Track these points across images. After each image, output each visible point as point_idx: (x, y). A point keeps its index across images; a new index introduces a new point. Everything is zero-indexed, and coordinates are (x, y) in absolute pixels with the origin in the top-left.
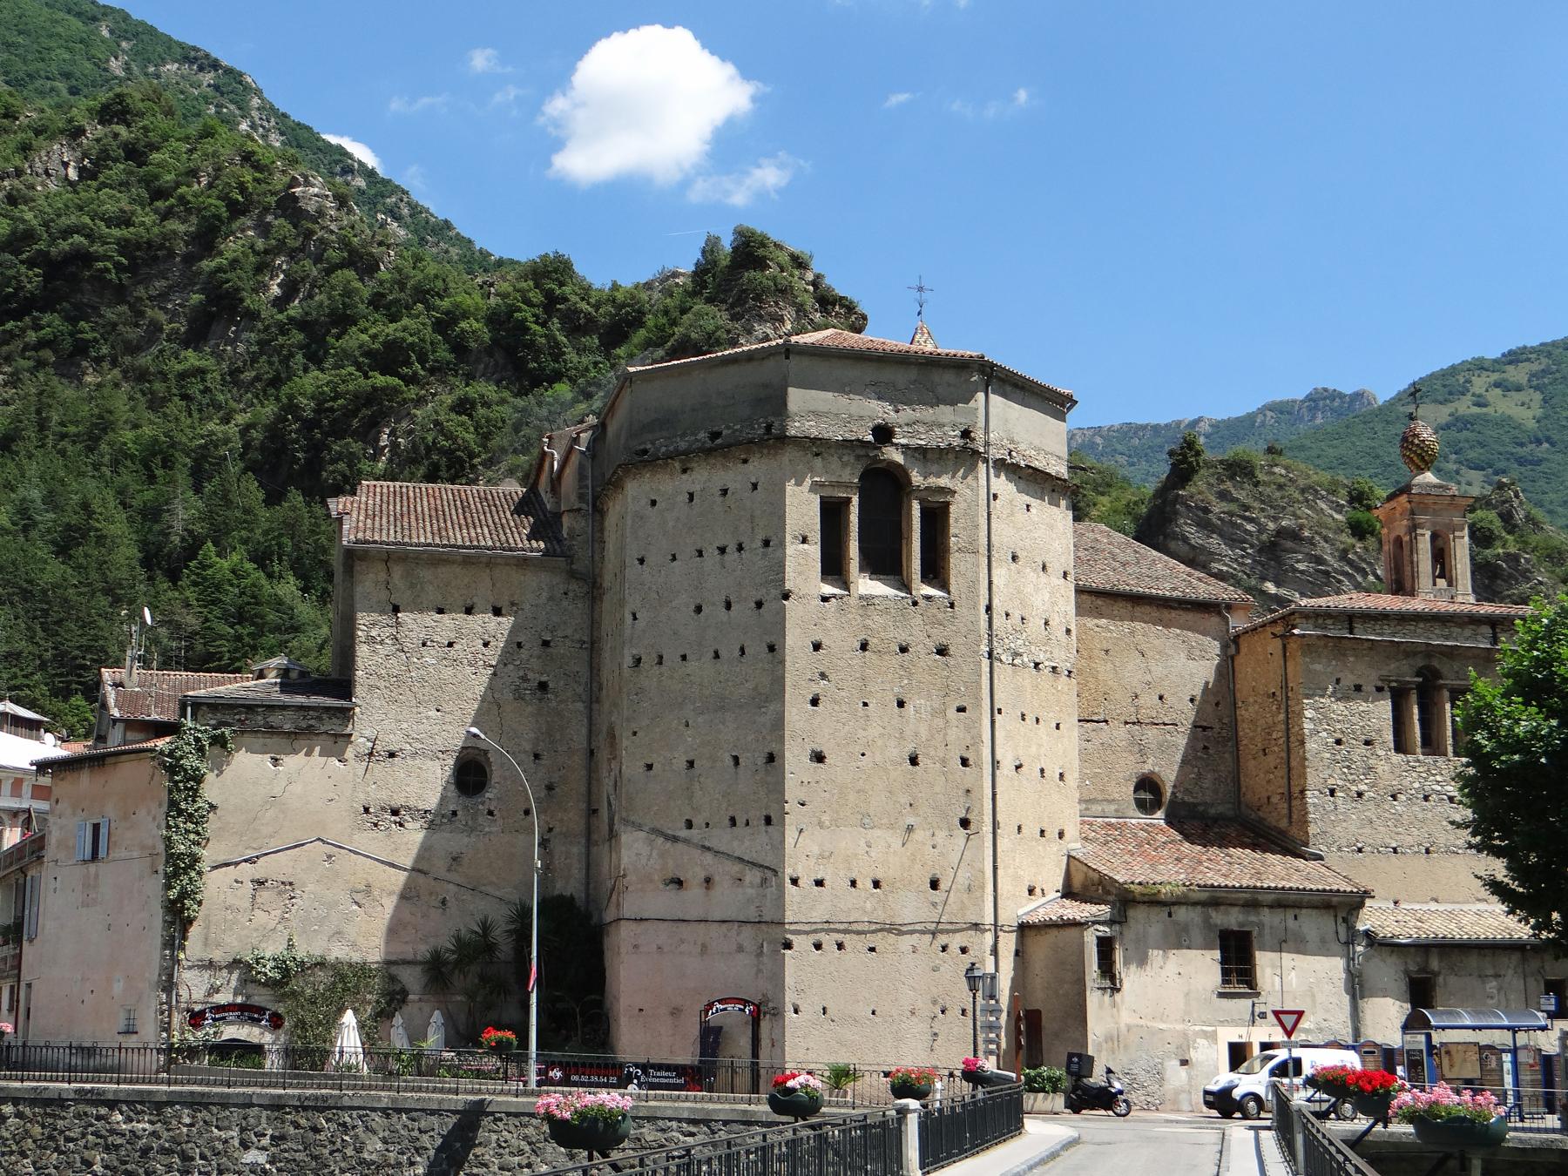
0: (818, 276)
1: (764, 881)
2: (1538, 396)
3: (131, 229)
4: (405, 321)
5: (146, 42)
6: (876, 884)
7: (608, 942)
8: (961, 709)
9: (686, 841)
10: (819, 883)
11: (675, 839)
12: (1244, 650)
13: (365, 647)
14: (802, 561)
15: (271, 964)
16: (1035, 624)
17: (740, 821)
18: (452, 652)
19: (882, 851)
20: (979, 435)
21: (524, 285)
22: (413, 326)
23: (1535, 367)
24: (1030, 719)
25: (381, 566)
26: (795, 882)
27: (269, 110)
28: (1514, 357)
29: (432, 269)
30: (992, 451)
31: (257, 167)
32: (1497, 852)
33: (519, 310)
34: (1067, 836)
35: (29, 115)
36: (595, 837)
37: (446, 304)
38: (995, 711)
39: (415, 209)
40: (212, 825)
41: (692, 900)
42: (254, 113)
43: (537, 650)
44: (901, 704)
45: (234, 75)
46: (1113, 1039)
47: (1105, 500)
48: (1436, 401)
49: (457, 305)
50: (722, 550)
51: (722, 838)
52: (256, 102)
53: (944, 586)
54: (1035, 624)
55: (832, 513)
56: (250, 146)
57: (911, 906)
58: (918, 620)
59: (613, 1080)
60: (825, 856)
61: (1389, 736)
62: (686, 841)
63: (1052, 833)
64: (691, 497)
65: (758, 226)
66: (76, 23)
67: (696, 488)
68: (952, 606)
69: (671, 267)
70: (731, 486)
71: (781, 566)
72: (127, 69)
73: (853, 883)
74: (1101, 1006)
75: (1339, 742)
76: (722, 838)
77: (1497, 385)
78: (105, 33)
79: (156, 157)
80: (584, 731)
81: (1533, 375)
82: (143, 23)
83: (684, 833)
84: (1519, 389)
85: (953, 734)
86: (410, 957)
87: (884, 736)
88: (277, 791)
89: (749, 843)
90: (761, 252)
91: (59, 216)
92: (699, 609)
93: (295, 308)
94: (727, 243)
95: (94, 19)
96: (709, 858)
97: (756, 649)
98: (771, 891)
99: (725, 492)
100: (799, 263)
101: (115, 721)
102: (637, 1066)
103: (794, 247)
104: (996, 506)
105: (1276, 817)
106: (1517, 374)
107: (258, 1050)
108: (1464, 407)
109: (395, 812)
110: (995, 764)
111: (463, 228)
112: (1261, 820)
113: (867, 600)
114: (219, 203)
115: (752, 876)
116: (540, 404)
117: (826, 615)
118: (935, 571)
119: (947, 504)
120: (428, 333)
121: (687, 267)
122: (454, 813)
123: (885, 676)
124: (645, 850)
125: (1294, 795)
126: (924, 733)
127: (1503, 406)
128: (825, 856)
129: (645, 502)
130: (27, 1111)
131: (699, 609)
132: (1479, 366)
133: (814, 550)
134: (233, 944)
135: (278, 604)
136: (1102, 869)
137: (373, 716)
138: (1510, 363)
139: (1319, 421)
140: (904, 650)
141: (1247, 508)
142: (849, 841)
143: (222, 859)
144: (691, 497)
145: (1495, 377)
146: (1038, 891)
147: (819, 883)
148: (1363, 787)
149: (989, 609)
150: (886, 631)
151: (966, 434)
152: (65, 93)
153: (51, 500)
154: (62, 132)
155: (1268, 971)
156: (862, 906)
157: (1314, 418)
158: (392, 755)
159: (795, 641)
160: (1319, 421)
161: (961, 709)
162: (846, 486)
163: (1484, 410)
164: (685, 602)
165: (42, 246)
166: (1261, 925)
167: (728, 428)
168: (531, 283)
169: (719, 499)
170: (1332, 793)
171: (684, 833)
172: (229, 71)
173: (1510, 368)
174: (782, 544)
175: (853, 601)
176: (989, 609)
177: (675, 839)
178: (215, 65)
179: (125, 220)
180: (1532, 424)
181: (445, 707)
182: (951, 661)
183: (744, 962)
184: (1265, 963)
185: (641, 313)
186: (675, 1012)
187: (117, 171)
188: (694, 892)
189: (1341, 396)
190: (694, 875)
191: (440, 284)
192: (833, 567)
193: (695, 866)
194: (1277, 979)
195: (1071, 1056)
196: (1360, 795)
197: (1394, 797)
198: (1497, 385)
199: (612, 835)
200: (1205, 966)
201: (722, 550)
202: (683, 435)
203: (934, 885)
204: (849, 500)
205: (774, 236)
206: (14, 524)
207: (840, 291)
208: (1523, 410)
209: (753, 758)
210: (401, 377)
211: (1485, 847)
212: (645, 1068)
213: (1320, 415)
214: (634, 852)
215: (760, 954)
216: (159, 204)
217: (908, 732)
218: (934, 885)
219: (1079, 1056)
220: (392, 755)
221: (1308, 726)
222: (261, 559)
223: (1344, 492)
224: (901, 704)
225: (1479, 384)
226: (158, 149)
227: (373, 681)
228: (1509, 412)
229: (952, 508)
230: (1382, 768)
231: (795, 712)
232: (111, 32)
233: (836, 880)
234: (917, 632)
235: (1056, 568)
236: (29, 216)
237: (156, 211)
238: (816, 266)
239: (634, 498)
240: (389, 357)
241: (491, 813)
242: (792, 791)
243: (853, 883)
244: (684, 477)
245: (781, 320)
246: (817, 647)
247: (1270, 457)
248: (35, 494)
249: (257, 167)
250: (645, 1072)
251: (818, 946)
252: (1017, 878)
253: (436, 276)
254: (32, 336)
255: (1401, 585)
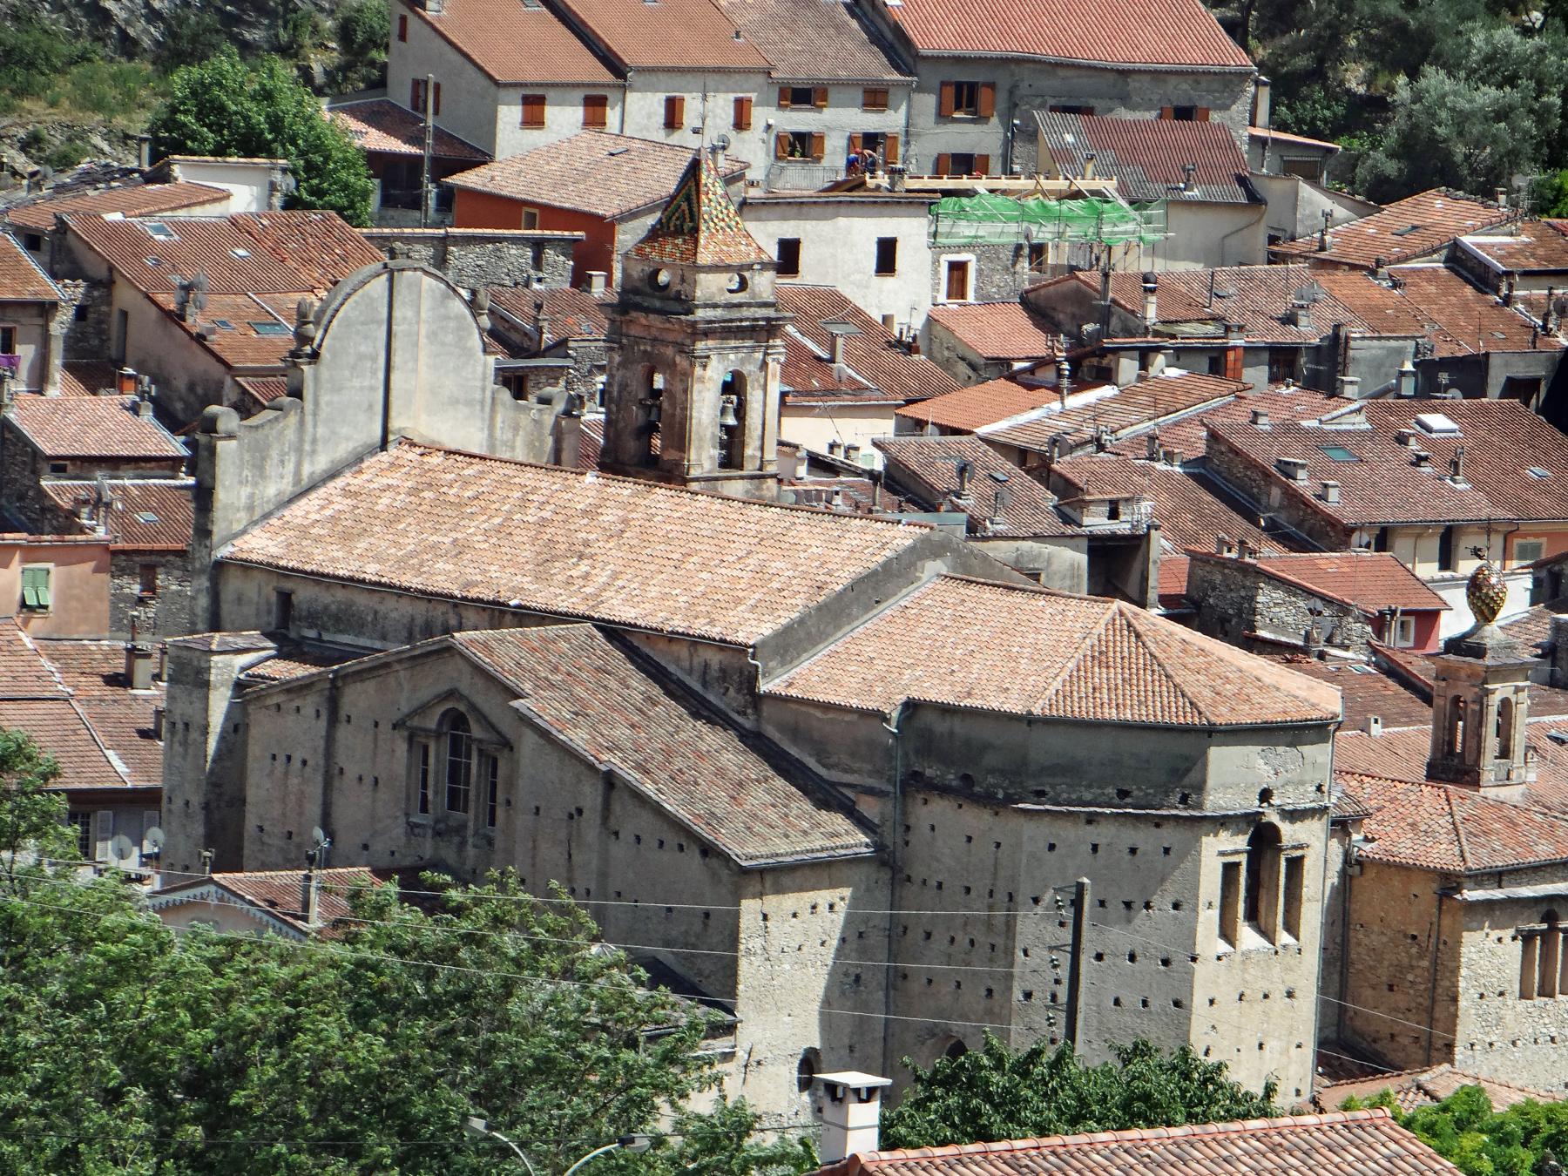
13: (740, 634)
14: (1208, 939)
25: (758, 878)
55: (1230, 870)
61: (1517, 987)
64: (1095, 848)
67: (1102, 841)
70: (1142, 848)
119: (1302, 858)
129: (1044, 845)
130: (620, 583)
133: (1215, 914)
144: (1095, 848)
148: (1494, 1038)
167: (1139, 789)
169: (1128, 857)
174: (1195, 910)
175: (1238, 958)
181: (796, 1012)
184: (550, 112)
192: (1227, 934)
197: (1514, 1043)
200: (577, 113)
202: (1089, 786)
230: (1509, 1016)
239: (1031, 838)
244: (1089, 828)
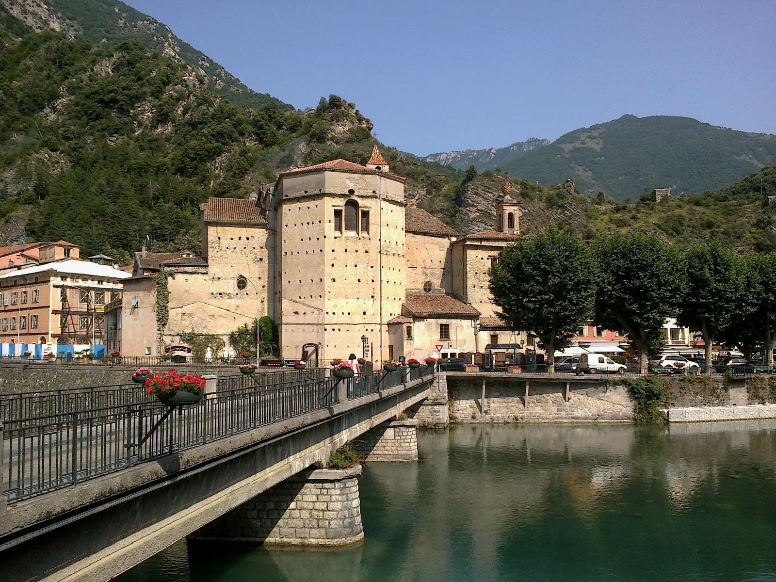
0: (357, 111)
1: (319, 313)
2: (601, 141)
3: (131, 91)
4: (223, 124)
5: (133, 15)
6: (349, 314)
7: (279, 329)
8: (372, 267)
9: (299, 302)
10: (334, 313)
11: (296, 302)
12: (454, 247)
15: (66, 45)
16: (393, 244)
17: (313, 297)
18: (235, 250)
19: (352, 305)
20: (378, 192)
21: (262, 113)
22: (227, 125)
23: (601, 131)
24: (392, 269)
26: (327, 313)
27: (175, 38)
28: (594, 128)
29: (232, 106)
30: (381, 196)
31: (172, 68)
32: (499, 305)
33: (260, 121)
34: (402, 300)
35: (95, 49)
36: (276, 300)
37: (236, 119)
38: (382, 267)
39: (227, 74)
40: (170, 297)
41: (300, 319)
42: (169, 39)
43: (259, 249)
44: (356, 266)
45: (162, 26)
46: (411, 353)
47: (447, 186)
48: (569, 143)
49: (239, 119)
50: (308, 223)
51: (308, 301)
52: (170, 35)
53: (368, 234)
54: (393, 244)
56: (170, 62)
57: (358, 319)
58: (361, 243)
59: (279, 365)
60: (335, 306)
62: (299, 302)
63: (397, 299)
64: (300, 208)
65: (338, 94)
66: (106, 7)
67: (301, 207)
68: (370, 239)
69: (309, 107)
71: (324, 228)
72: (125, 24)
73: (343, 313)
74: (407, 343)
75: (476, 273)
76: (308, 301)
77: (588, 137)
78: (117, 10)
79: (138, 65)
80: (273, 272)
81: (601, 134)
82: (129, 7)
83: (299, 300)
84: (595, 138)
85: (370, 274)
86: (226, 333)
87: (352, 274)
88: (188, 289)
89: (316, 303)
90: (338, 103)
91: (106, 86)
92: (302, 240)
93: (188, 116)
94: (327, 100)
95: (112, 5)
96: (305, 307)
97: (317, 251)
98: (321, 316)
99: (309, 208)
100: (351, 106)
101: (140, 268)
102: (286, 361)
103: (349, 101)
104: (383, 212)
105: (460, 293)
106: (595, 133)
107: (185, 358)
108: (578, 145)
109: (220, 294)
110: (381, 281)
111: (243, 81)
112: (457, 294)
113: (347, 238)
114: (160, 82)
115: (316, 312)
116: (268, 153)
117: (336, 241)
118: (366, 228)
120: (231, 128)
121: (315, 108)
122: (237, 294)
123: (351, 258)
124: (288, 304)
125: (465, 287)
126: (362, 273)
127: (590, 144)
128: (335, 306)
131: (302, 240)
132: (583, 130)
134: (176, 330)
135: (185, 218)
136: (410, 308)
137: (214, 268)
138: (593, 129)
139: (531, 149)
140: (357, 251)
141: (489, 189)
142: (342, 302)
143: (172, 307)
145: (588, 134)
146: (393, 315)
147: (334, 313)
148: (482, 285)
149: (380, 240)
150: (352, 246)
151: (374, 192)
152: (104, 32)
153: (109, 183)
154: (106, 56)
155: (453, 335)
156: (345, 319)
157: (530, 147)
158: (219, 279)
159: (327, 249)
160: (531, 149)
161: (372, 267)
162: (342, 206)
163: (584, 146)
164: (298, 238)
165: (101, 96)
166: (451, 323)
168: (264, 112)
170: (474, 287)
171: (299, 300)
172: (160, 24)
173: (593, 131)
176: (380, 240)
177: (296, 302)
178: (156, 22)
179: (128, 88)
180: (599, 150)
182: (369, 254)
183: (314, 335)
185: (300, 122)
186: (297, 347)
187: (125, 70)
188: (301, 316)
189: (539, 140)
190: (301, 311)
191: (234, 111)
193: (301, 309)
194: (455, 337)
195: (400, 357)
196: (482, 287)
198: (588, 137)
199: (280, 301)
201: (308, 223)
203: (364, 313)
204: (342, 210)
205: (343, 98)
206: (97, 192)
207: (365, 116)
208: (596, 146)
209: (316, 280)
210: (222, 143)
211: (497, 303)
212: (288, 362)
213: (531, 147)
214: (286, 305)
215: (318, 332)
216: (140, 82)
217: (358, 273)
218: (364, 313)
219: (403, 357)
220: (219, 279)
221: (468, 269)
222: (178, 203)
223: (519, 183)
224: (356, 266)
225: (583, 137)
226: (139, 62)
227: (213, 258)
228: (592, 146)
229: (370, 212)
231: (327, 268)
232: (119, 10)
233: (339, 313)
234: (360, 246)
235: (400, 228)
236: (96, 86)
237: (139, 85)
238: (356, 108)
240: (219, 136)
241: (247, 294)
242: (327, 289)
243: (343, 313)
245: (345, 126)
246: (333, 251)
247: (497, 172)
248: (104, 182)
249: (172, 68)
250: (288, 363)
251: (333, 330)
252: (387, 311)
253: (233, 109)
254: (99, 127)
255: (500, 229)
